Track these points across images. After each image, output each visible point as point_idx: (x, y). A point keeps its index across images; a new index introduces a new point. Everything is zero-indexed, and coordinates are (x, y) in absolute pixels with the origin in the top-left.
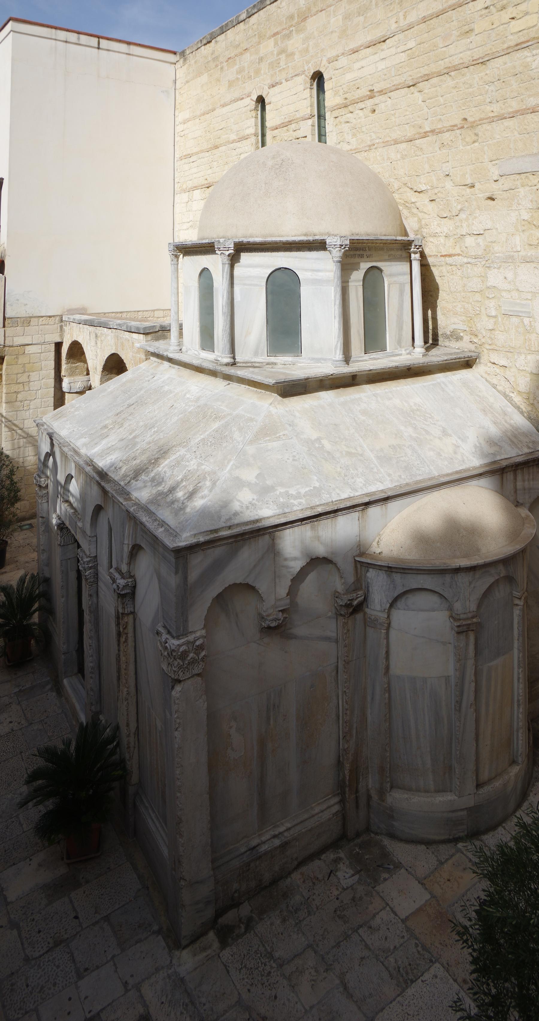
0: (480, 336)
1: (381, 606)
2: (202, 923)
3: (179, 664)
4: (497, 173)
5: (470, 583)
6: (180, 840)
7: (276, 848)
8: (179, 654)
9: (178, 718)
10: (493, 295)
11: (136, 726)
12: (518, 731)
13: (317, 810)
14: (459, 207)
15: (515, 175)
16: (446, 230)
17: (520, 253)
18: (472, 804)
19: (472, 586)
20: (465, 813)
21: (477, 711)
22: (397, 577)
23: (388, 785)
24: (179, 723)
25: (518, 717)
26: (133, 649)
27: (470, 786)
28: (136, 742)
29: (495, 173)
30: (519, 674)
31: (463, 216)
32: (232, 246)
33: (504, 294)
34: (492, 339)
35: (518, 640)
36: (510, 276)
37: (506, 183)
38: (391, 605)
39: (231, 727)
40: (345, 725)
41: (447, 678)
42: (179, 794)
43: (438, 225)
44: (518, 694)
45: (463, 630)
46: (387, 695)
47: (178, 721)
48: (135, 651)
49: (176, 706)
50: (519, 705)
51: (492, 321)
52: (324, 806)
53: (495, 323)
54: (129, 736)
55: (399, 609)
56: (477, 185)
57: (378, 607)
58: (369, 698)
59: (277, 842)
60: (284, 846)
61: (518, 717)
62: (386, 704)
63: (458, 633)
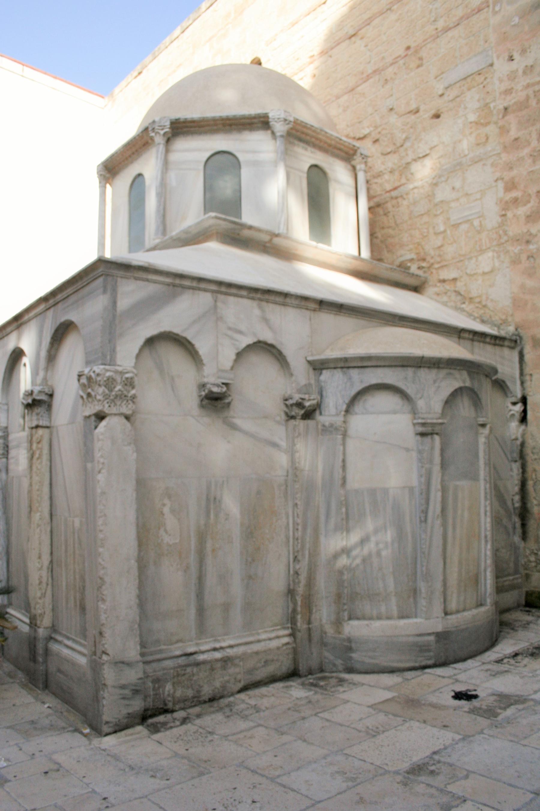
0: (428, 258)
1: (336, 408)
2: (129, 714)
3: (104, 392)
4: (442, 87)
5: (435, 382)
6: (102, 606)
7: (217, 660)
8: (105, 379)
9: (102, 456)
10: (441, 210)
11: (49, 560)
12: (485, 571)
13: (264, 636)
14: (404, 136)
15: (461, 82)
16: (390, 165)
17: (468, 157)
18: (439, 628)
19: (437, 385)
20: (432, 638)
21: (444, 525)
22: (354, 373)
23: (346, 614)
24: (103, 463)
25: (486, 555)
26: (48, 469)
27: (438, 609)
28: (50, 579)
29: (440, 87)
30: (486, 506)
31: (408, 144)
32: (168, 124)
33: (453, 205)
34: (440, 256)
35: (485, 470)
36: (458, 185)
37: (452, 94)
38: (347, 411)
39: (164, 505)
40: (296, 543)
41: (411, 489)
42: (101, 550)
43: (383, 163)
44: (486, 529)
45: (426, 432)
46: (344, 510)
47: (102, 460)
48: (51, 472)
49: (100, 442)
50: (486, 541)
51: (440, 237)
52: (273, 635)
53: (444, 239)
54: (41, 569)
55: (356, 414)
56: (422, 108)
57: (333, 411)
58: (323, 518)
59: (218, 655)
60: (226, 661)
61: (486, 555)
62: (342, 519)
63: (423, 434)
